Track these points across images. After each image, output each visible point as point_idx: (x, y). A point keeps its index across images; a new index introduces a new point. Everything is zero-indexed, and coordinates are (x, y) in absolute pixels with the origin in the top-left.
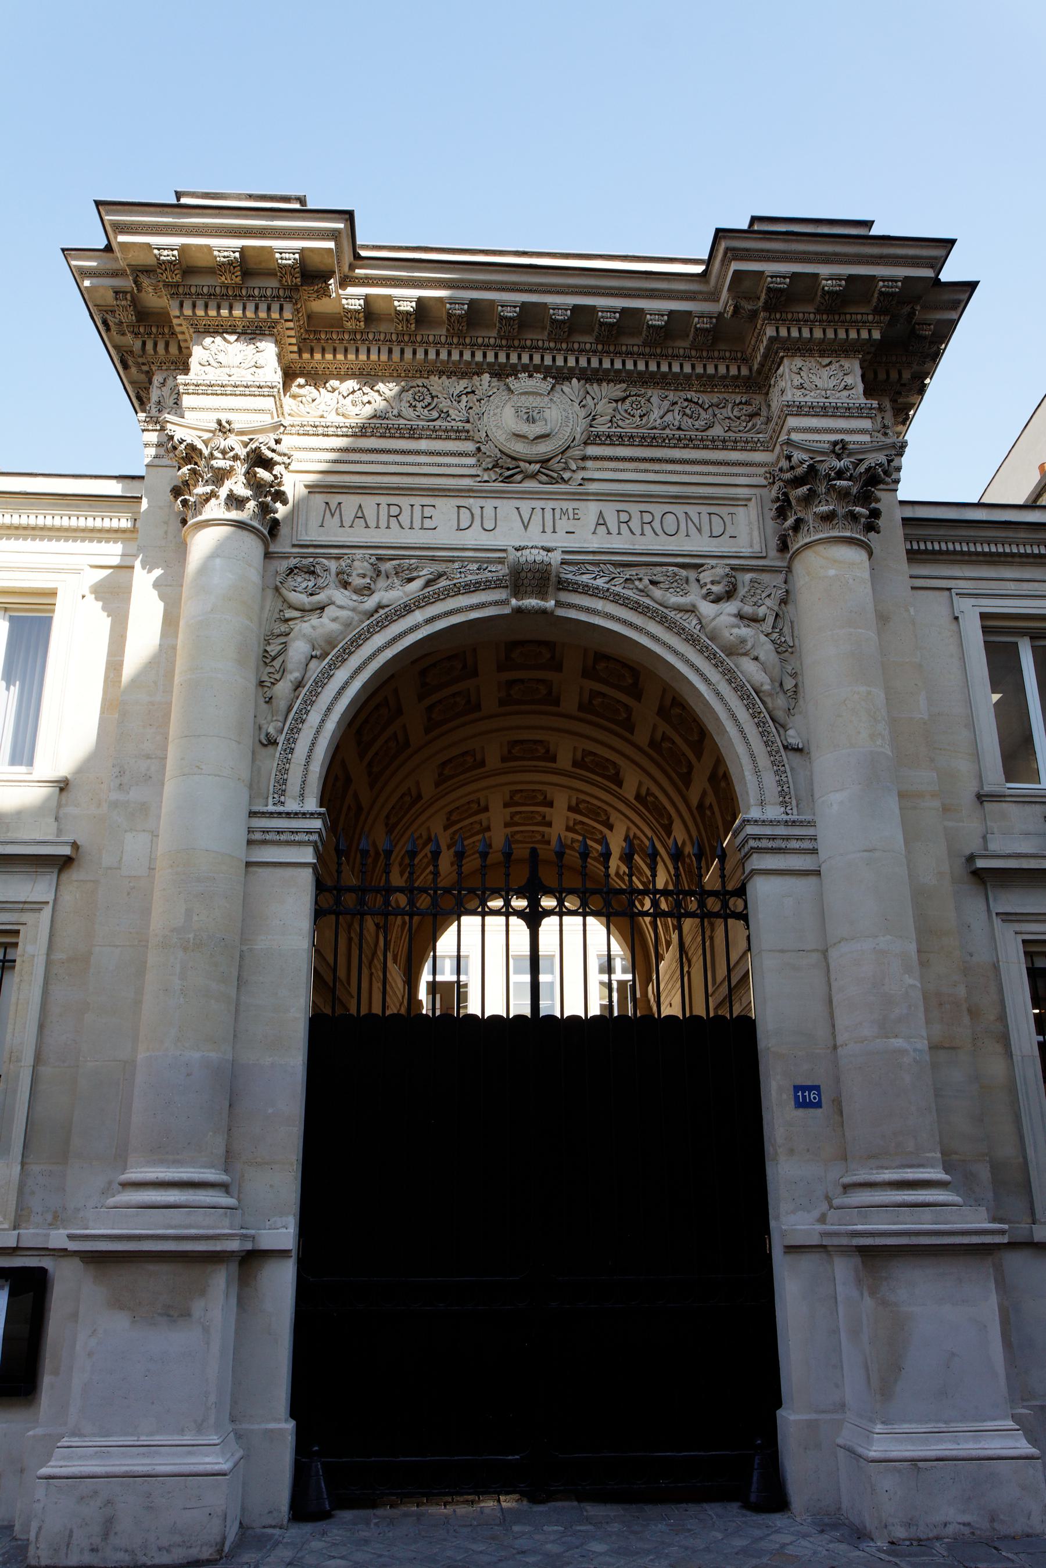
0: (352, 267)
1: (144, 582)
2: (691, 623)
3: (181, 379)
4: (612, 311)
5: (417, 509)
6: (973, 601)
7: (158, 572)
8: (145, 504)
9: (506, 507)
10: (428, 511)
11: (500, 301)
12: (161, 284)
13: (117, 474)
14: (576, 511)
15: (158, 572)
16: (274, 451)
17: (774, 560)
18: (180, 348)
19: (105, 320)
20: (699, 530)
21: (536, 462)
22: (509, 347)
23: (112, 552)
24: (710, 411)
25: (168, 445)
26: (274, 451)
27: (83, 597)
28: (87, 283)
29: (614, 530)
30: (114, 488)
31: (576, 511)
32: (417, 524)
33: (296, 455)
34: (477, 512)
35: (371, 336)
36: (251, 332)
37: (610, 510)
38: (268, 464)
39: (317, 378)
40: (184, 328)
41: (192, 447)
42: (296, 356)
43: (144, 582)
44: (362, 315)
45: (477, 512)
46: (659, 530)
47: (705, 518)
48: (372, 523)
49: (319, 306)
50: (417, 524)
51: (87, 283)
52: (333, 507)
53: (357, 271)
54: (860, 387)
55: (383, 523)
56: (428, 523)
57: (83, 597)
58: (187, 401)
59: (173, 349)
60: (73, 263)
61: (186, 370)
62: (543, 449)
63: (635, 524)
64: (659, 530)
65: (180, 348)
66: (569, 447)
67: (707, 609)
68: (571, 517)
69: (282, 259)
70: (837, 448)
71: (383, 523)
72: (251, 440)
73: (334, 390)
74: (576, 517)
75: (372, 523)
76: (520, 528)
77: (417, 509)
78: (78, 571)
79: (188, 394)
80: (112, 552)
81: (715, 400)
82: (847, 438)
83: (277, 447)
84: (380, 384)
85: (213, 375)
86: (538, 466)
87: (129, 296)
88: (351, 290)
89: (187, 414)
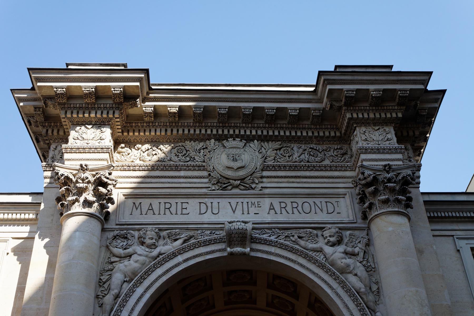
0: (148, 94)
1: (39, 245)
2: (321, 258)
3: (64, 146)
4: (272, 109)
5: (179, 204)
6: (466, 242)
7: (47, 240)
8: (42, 206)
9: (224, 202)
10: (185, 206)
11: (290, 108)
12: (57, 104)
13: (30, 192)
14: (259, 203)
15: (47, 240)
16: (108, 178)
17: (360, 224)
18: (64, 132)
19: (29, 120)
20: (322, 210)
21: (238, 180)
22: (223, 127)
23: (24, 231)
24: (323, 153)
25: (56, 177)
26: (108, 178)
27: (8, 254)
28: (21, 104)
29: (278, 212)
30: (28, 199)
31: (259, 203)
32: (179, 212)
33: (119, 180)
34: (209, 205)
35: (157, 124)
36: (99, 124)
37: (276, 202)
38: (105, 185)
39: (131, 144)
40: (67, 123)
41: (67, 178)
42: (120, 134)
43: (39, 245)
44: (152, 114)
45: (209, 205)
46: (301, 211)
47: (324, 204)
48: (157, 212)
49: (132, 111)
50: (179, 212)
51: (21, 104)
52: (137, 205)
53: (150, 95)
54: (395, 139)
55: (162, 212)
56: (184, 211)
57: (8, 254)
58: (66, 156)
59: (61, 133)
60: (16, 95)
61: (67, 142)
62: (241, 173)
63: (289, 208)
64: (301, 211)
65: (64, 132)
66: (254, 172)
67: (328, 250)
68: (257, 206)
69: (114, 91)
70: (387, 168)
71: (162, 212)
72: (97, 173)
73: (138, 149)
74: (259, 206)
75: (157, 212)
76: (229, 213)
77: (179, 204)
78: (6, 241)
79: (67, 153)
80: (24, 231)
81: (325, 148)
82: (391, 163)
83: (110, 177)
84: (161, 146)
85: (79, 144)
86: (239, 182)
87: (41, 110)
88: (147, 104)
89: (66, 162)
